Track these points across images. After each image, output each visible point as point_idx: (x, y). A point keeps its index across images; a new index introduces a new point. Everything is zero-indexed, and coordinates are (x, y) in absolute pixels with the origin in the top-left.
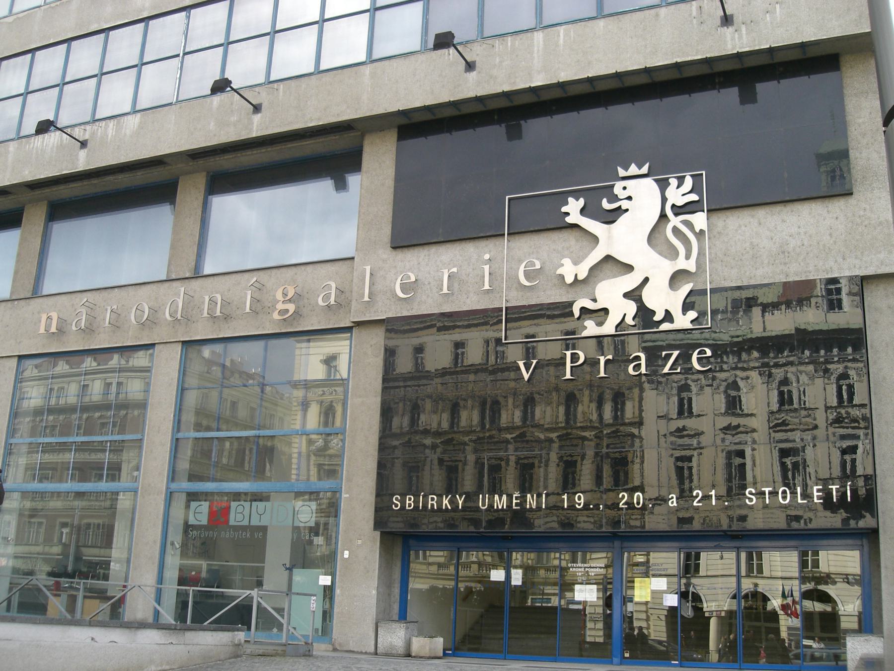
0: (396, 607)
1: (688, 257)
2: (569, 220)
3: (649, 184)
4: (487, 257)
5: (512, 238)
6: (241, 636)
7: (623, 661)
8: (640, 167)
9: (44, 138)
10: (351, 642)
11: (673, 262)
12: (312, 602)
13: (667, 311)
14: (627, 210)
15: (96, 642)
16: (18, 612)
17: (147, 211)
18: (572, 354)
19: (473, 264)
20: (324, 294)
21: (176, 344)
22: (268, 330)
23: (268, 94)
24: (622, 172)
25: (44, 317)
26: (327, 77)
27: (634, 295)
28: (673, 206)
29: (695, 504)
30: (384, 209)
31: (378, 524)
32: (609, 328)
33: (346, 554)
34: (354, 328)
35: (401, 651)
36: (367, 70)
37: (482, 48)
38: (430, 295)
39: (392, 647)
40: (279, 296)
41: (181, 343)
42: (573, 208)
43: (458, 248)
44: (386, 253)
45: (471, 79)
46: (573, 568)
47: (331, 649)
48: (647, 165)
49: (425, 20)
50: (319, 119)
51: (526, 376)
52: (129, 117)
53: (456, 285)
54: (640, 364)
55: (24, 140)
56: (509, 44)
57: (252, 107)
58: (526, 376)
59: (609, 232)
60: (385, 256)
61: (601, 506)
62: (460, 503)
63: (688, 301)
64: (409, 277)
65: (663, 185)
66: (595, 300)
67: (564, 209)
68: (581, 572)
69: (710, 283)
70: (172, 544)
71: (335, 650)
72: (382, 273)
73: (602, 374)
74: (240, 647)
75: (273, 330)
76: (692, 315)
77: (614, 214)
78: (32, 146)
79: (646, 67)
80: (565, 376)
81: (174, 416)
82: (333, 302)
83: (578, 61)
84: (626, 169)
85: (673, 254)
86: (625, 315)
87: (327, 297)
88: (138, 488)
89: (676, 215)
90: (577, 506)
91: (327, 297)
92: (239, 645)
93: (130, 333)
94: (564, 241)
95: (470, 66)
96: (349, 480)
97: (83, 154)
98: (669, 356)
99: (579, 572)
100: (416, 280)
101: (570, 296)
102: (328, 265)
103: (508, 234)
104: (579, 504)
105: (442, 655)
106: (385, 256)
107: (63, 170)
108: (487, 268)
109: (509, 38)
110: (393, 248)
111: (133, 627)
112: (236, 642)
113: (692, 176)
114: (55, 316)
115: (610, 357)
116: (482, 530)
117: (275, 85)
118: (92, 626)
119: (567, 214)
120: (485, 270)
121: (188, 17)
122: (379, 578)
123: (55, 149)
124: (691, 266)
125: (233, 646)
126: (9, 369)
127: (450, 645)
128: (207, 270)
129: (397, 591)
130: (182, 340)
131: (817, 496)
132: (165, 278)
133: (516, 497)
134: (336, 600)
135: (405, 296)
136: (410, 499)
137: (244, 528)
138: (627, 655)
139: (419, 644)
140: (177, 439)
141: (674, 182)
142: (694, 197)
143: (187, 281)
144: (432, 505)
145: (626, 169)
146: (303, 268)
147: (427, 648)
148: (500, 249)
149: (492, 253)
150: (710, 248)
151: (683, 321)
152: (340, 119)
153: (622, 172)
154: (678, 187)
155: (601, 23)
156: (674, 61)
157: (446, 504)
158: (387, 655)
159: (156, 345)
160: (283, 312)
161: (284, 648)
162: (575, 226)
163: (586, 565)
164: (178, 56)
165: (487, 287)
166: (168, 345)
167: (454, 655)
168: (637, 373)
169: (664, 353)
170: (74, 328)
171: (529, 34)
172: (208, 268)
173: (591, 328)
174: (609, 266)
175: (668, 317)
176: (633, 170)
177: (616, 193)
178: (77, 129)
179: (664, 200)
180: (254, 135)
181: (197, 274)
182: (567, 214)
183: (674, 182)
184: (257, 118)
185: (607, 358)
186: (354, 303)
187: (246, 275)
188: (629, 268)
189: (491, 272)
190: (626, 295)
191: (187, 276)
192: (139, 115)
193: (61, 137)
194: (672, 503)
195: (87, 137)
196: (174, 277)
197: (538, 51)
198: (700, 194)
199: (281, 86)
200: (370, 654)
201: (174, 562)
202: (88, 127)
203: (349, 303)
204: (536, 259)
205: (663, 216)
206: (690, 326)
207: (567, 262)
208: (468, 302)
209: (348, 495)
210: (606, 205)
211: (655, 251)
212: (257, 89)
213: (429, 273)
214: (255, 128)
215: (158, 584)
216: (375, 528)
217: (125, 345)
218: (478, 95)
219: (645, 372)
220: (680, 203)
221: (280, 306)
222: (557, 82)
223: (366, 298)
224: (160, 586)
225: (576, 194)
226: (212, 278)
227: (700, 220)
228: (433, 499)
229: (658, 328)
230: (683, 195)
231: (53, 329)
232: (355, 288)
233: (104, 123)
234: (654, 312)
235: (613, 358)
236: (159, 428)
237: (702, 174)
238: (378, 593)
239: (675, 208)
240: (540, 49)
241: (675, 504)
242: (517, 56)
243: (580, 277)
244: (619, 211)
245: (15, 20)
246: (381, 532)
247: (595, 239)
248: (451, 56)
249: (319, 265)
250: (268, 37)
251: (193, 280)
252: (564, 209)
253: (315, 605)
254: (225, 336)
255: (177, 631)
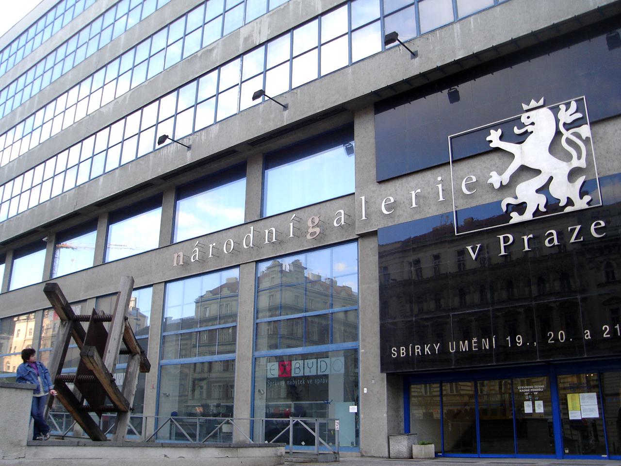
0: (402, 425)
1: (579, 158)
2: (492, 145)
3: (546, 112)
4: (439, 179)
5: (455, 164)
6: (282, 450)
7: (564, 456)
8: (537, 101)
9: (168, 148)
10: (372, 450)
11: (569, 163)
12: (336, 424)
13: (568, 198)
14: (532, 132)
15: (168, 457)
16: (176, 439)
17: (292, 165)
18: (504, 237)
19: (432, 185)
20: (336, 219)
21: (252, 263)
22: (306, 247)
23: (291, 97)
24: (525, 107)
25: (176, 256)
26: (325, 80)
27: (543, 190)
28: (565, 124)
29: (605, 336)
30: (370, 159)
31: (384, 367)
32: (528, 216)
33: (365, 390)
34: (359, 239)
35: (406, 455)
36: (350, 69)
37: (420, 41)
38: (405, 210)
39: (399, 452)
40: (310, 224)
41: (255, 263)
42: (494, 138)
43: (421, 176)
44: (375, 187)
45: (416, 63)
46: (522, 389)
47: (360, 456)
48: (542, 99)
49: (383, 32)
50: (323, 107)
51: (474, 257)
52: (213, 126)
53: (422, 201)
54: (553, 238)
55: (157, 151)
56: (438, 35)
57: (282, 107)
58: (474, 257)
59: (521, 149)
60: (374, 189)
61: (535, 343)
62: (437, 349)
63: (581, 191)
64: (390, 200)
65: (555, 110)
66: (516, 198)
67: (488, 139)
68: (528, 392)
69: (598, 174)
70: (259, 391)
71: (362, 456)
72: (373, 200)
73: (527, 249)
74: (282, 457)
75: (309, 246)
76: (587, 198)
77: (523, 136)
78: (162, 154)
79: (532, 32)
80: (501, 253)
81: (254, 309)
82: (343, 223)
83: (485, 37)
84: (528, 105)
85: (568, 157)
86: (538, 205)
87: (339, 221)
88: (236, 357)
89: (567, 130)
90: (518, 344)
91: (339, 221)
92: (281, 456)
93: (225, 260)
94: (491, 160)
95: (414, 55)
96: (364, 340)
97: (189, 154)
98: (573, 230)
99: (526, 392)
100: (477, 181)
101: (499, 197)
102: (339, 200)
103: (452, 162)
104: (519, 343)
105: (434, 456)
106: (374, 189)
107: (179, 166)
108: (440, 186)
109: (438, 32)
110: (377, 182)
111: (196, 447)
112: (279, 454)
113: (576, 101)
114: (181, 254)
115: (531, 236)
116: (453, 367)
117: (295, 91)
118: (164, 447)
119: (491, 141)
120: (439, 187)
121: (242, 61)
122: (388, 405)
123: (174, 154)
124: (582, 163)
125: (276, 457)
126: (160, 290)
127: (440, 449)
128: (268, 213)
129: (402, 413)
130: (255, 260)
131: (474, 346)
132: (243, 223)
133: (474, 342)
134: (361, 422)
135: (389, 213)
136: (403, 350)
137: (301, 378)
138: (567, 451)
139: (417, 449)
140: (257, 324)
141: (563, 107)
142: (579, 115)
143: (255, 223)
144: (418, 352)
145: (528, 105)
146: (324, 204)
147: (423, 452)
148: (449, 172)
149: (443, 176)
150: (595, 150)
151: (581, 204)
152: (336, 105)
153: (525, 107)
154: (566, 110)
155: (498, 9)
156: (552, 23)
157: (427, 351)
158: (397, 458)
159: (241, 265)
160: (312, 234)
161: (316, 457)
162: (497, 150)
163: (530, 387)
164: (238, 84)
165: (441, 199)
166: (248, 264)
167: (444, 456)
168: (551, 245)
169: (569, 228)
170: (192, 260)
171: (451, 26)
172: (269, 212)
173: (516, 218)
174: (525, 174)
175: (570, 202)
176: (533, 103)
177: (522, 122)
178: (185, 139)
179: (557, 121)
180: (285, 124)
181: (262, 218)
182: (491, 141)
183: (563, 107)
184: (286, 113)
185: (529, 236)
186: (357, 221)
187: (290, 214)
188: (538, 172)
189: (444, 189)
190: (538, 191)
191: (256, 219)
192: (218, 124)
193: (177, 146)
194: (587, 336)
195: (191, 143)
196: (248, 221)
197: (458, 36)
198: (583, 112)
199: (299, 90)
200: (385, 457)
201: (261, 403)
202: (191, 137)
203: (354, 223)
204: (473, 175)
205: (558, 133)
206: (587, 207)
207: (494, 174)
208: (430, 211)
209: (363, 351)
210: (517, 131)
211: (556, 158)
212: (284, 95)
213: (403, 196)
214: (285, 120)
215: (251, 418)
216: (382, 371)
217: (223, 267)
218: (421, 72)
219: (557, 244)
220: (569, 120)
221: (311, 230)
222: (472, 53)
223: (364, 218)
224: (253, 419)
225: (495, 127)
226: (270, 219)
227: (585, 131)
228: (418, 348)
229: (563, 211)
230: (571, 115)
231: (181, 263)
232: (357, 212)
233: (199, 133)
234: (559, 200)
235: (533, 236)
236: (246, 317)
237: (583, 98)
238: (388, 416)
239: (566, 125)
240: (459, 34)
241: (589, 337)
242: (444, 42)
243: (504, 184)
244: (527, 134)
245: (149, 83)
246: (387, 374)
247: (511, 156)
248: (401, 51)
249: (334, 201)
250: (317, 49)
251: (259, 222)
252: (488, 139)
253: (338, 426)
254: (281, 254)
255: (231, 448)
